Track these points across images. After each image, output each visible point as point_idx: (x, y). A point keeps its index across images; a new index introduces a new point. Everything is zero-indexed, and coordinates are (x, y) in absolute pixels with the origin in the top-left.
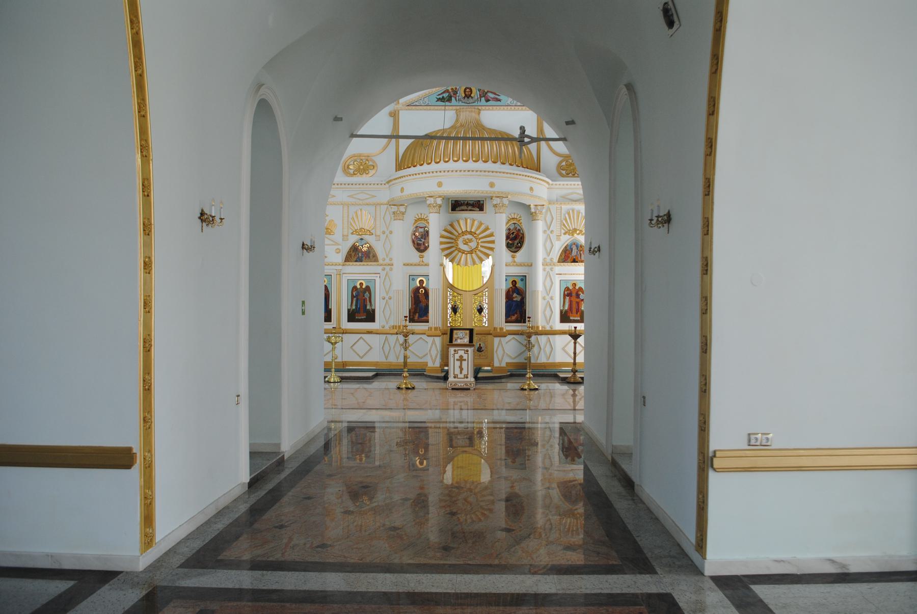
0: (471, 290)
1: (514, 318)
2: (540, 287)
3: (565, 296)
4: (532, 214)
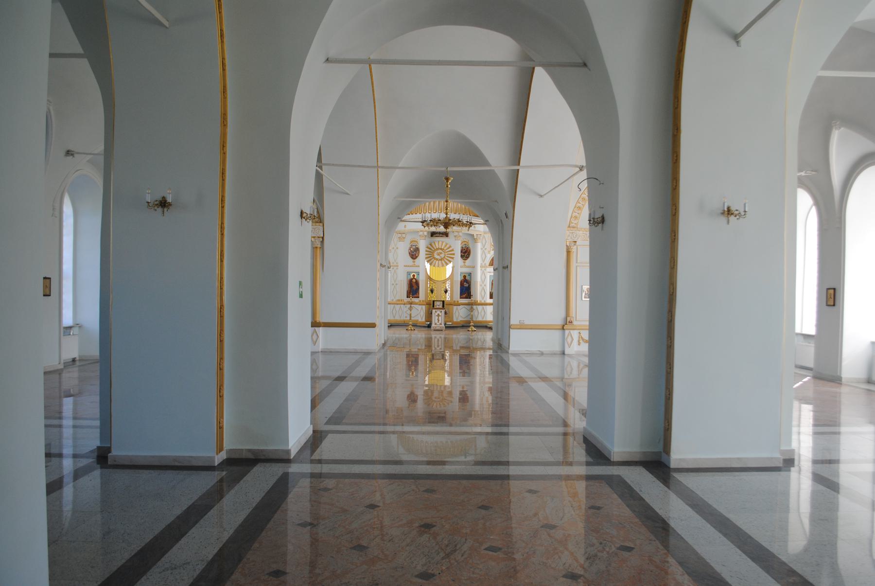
1: (464, 296)
4: (475, 239)
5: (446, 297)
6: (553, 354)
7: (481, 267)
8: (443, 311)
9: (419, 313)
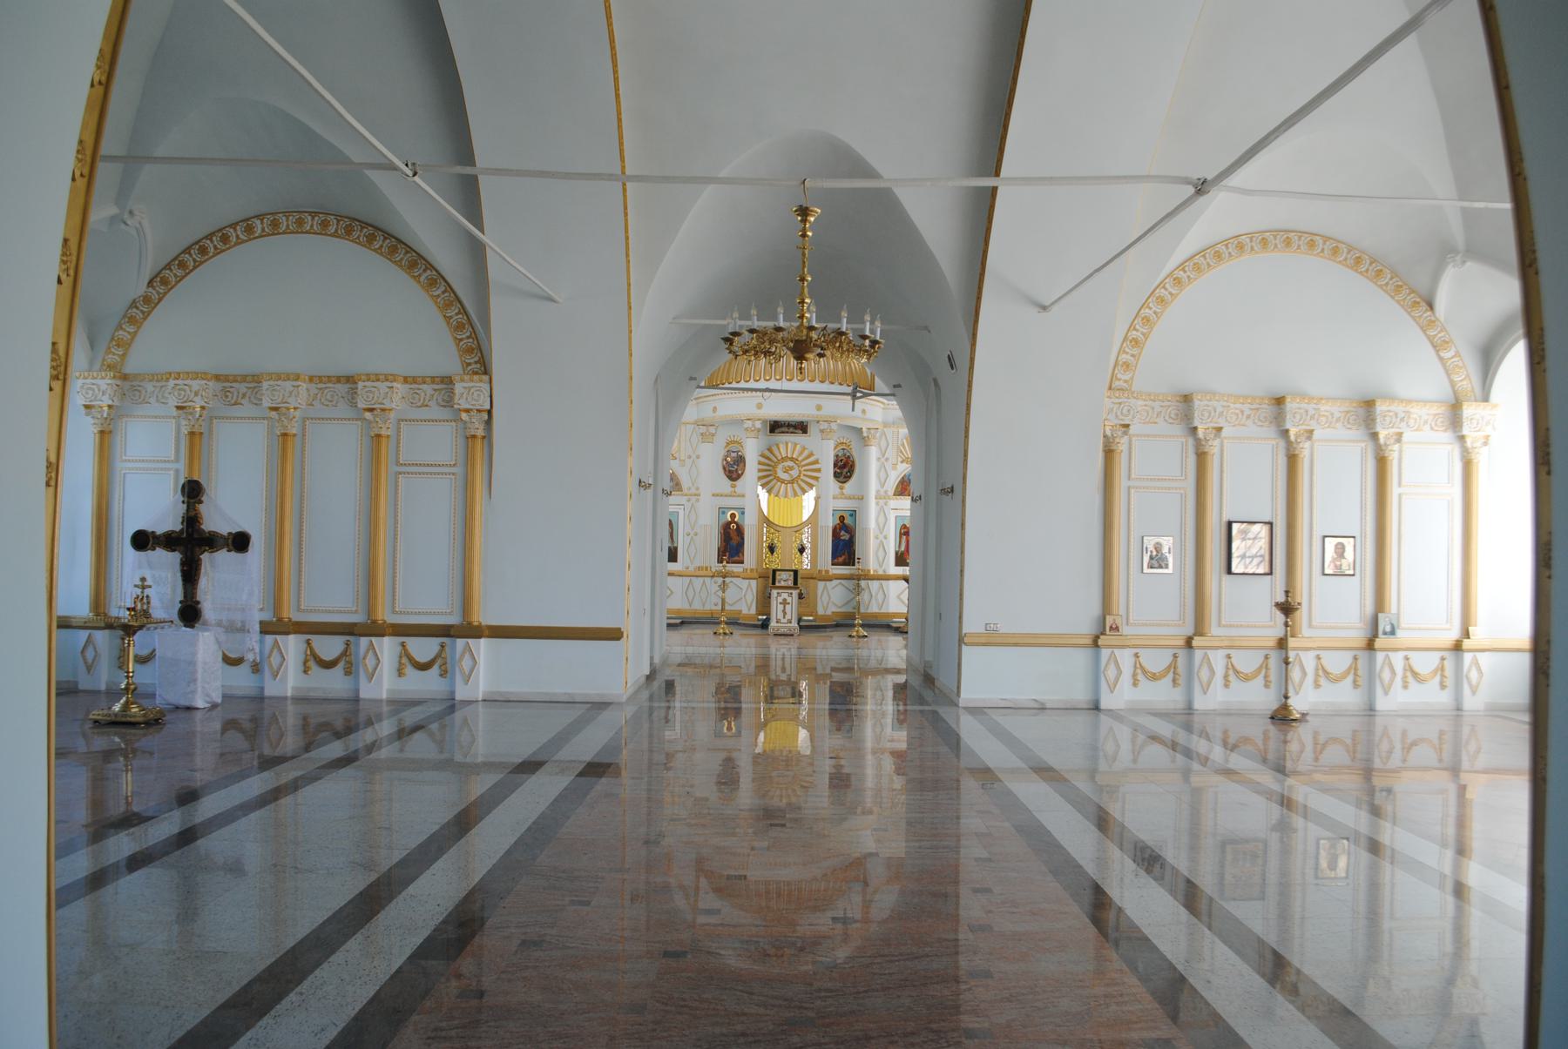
0: (789, 525)
2: (872, 525)
3: (901, 534)
4: (864, 438)
5: (802, 562)
6: (1071, 709)
7: (876, 498)
8: (795, 593)
9: (742, 597)
